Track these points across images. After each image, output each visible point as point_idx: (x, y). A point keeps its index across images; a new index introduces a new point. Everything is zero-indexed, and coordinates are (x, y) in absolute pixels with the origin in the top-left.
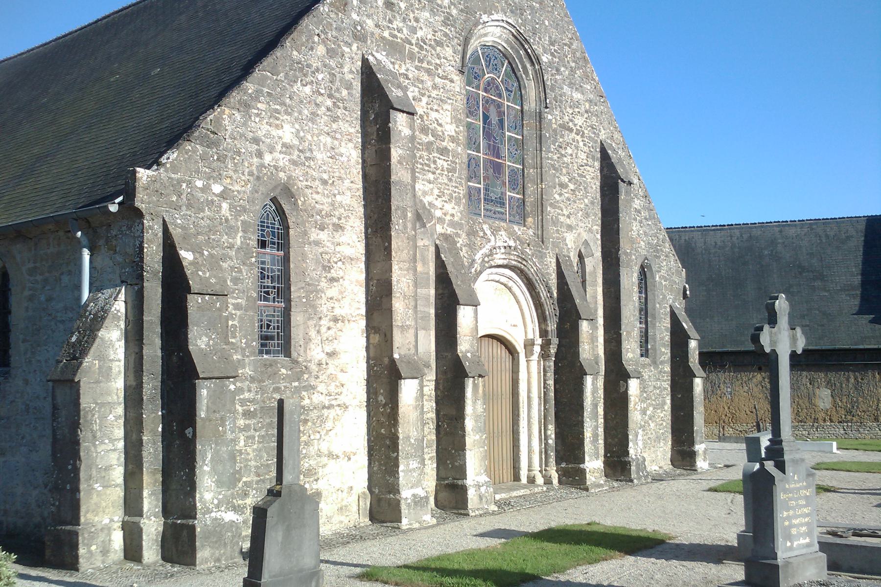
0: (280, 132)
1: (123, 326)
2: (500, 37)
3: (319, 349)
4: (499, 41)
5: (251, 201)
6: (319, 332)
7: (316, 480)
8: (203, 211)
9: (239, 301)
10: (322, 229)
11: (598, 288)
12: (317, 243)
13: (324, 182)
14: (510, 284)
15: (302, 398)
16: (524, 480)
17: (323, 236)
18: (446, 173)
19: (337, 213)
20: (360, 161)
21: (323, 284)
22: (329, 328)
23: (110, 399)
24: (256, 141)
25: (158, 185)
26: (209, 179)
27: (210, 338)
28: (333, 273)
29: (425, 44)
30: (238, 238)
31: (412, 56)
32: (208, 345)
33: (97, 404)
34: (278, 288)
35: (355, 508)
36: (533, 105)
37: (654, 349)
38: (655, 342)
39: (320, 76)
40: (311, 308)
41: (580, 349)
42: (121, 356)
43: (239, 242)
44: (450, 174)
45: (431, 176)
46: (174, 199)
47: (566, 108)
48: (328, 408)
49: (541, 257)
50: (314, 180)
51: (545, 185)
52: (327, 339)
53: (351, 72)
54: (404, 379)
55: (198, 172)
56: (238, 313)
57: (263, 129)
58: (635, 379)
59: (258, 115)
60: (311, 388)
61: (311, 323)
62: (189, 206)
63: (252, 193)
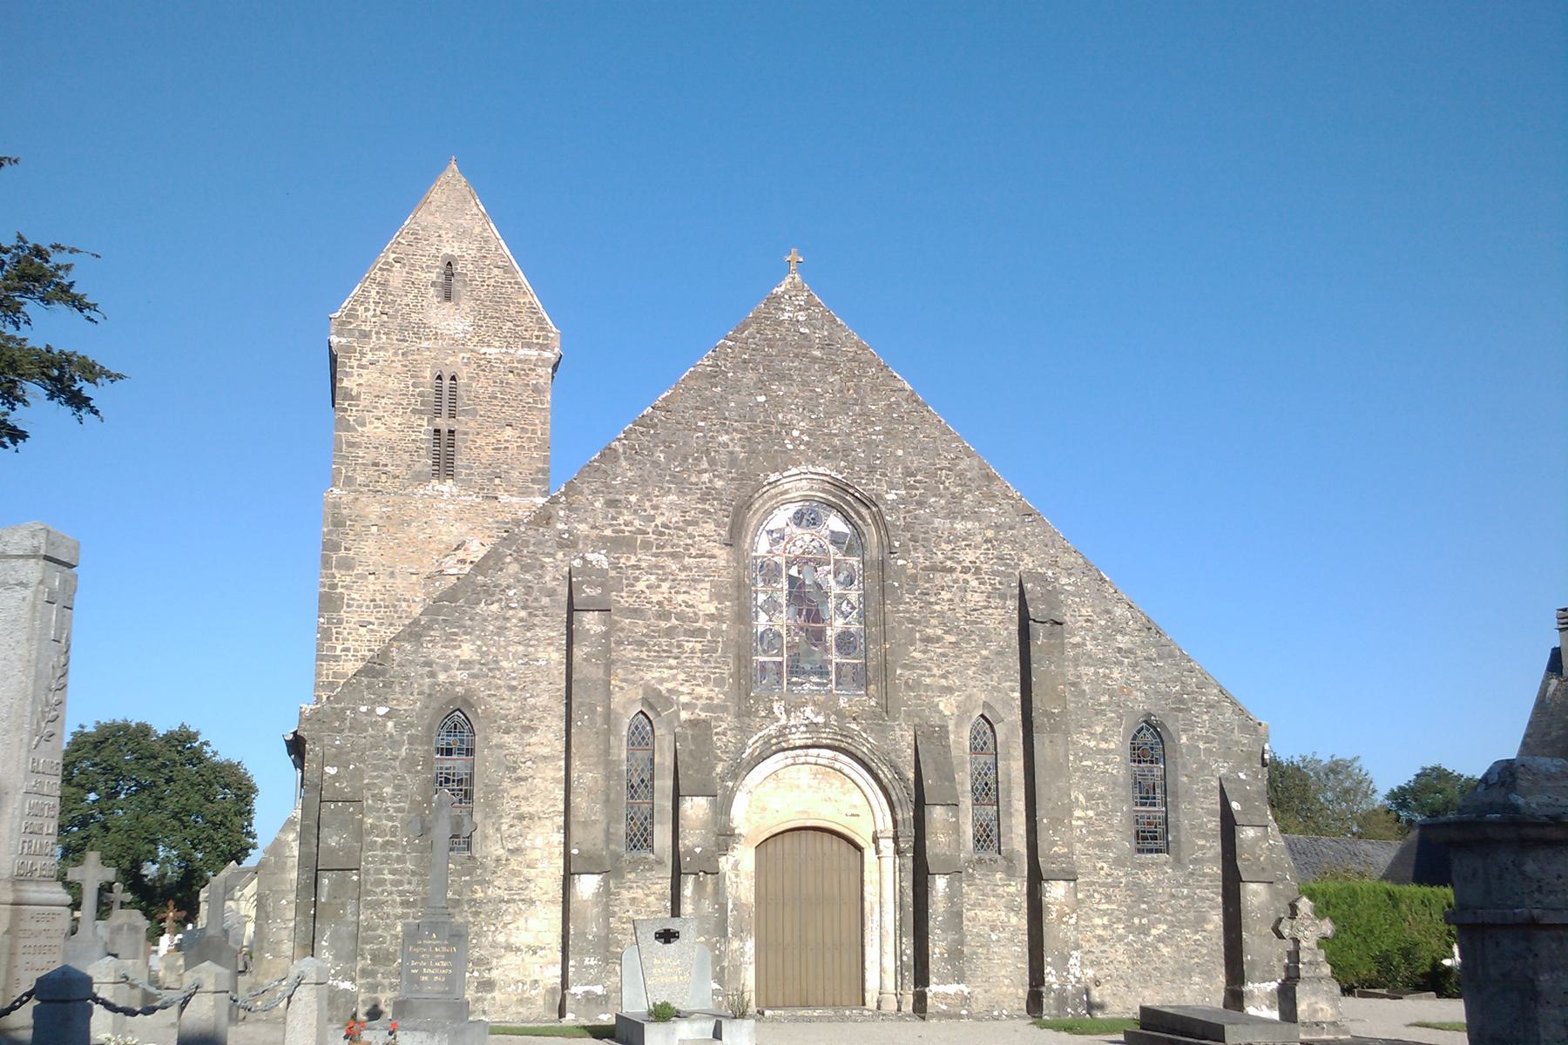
0: (458, 652)
1: (299, 830)
2: (811, 489)
3: (499, 846)
4: (813, 493)
5: (420, 716)
6: (498, 830)
7: (489, 970)
8: (366, 731)
9: (402, 804)
10: (507, 732)
11: (1012, 763)
12: (500, 746)
13: (513, 689)
14: (837, 765)
15: (475, 892)
16: (871, 1003)
17: (507, 739)
18: (699, 655)
19: (528, 716)
20: (565, 661)
21: (506, 784)
22: (511, 826)
23: (284, 888)
24: (428, 664)
25: (320, 716)
26: (374, 703)
27: (341, 837)
28: (520, 773)
29: (669, 528)
30: (403, 750)
31: (646, 545)
32: (338, 843)
33: (271, 890)
34: (466, 790)
35: (541, 1002)
36: (875, 553)
37: (1177, 841)
38: (1178, 831)
39: (511, 593)
40: (492, 808)
41: (927, 842)
42: (296, 853)
43: (404, 754)
44: (705, 655)
45: (673, 662)
46: (337, 724)
47: (938, 545)
48: (508, 902)
50: (499, 687)
51: (891, 644)
52: (509, 836)
53: (555, 579)
54: (1047, 880)
55: (362, 699)
56: (400, 815)
57: (435, 652)
58: (1062, 882)
59: (430, 641)
60: (485, 883)
61: (489, 822)
62: (351, 728)
63: (421, 709)
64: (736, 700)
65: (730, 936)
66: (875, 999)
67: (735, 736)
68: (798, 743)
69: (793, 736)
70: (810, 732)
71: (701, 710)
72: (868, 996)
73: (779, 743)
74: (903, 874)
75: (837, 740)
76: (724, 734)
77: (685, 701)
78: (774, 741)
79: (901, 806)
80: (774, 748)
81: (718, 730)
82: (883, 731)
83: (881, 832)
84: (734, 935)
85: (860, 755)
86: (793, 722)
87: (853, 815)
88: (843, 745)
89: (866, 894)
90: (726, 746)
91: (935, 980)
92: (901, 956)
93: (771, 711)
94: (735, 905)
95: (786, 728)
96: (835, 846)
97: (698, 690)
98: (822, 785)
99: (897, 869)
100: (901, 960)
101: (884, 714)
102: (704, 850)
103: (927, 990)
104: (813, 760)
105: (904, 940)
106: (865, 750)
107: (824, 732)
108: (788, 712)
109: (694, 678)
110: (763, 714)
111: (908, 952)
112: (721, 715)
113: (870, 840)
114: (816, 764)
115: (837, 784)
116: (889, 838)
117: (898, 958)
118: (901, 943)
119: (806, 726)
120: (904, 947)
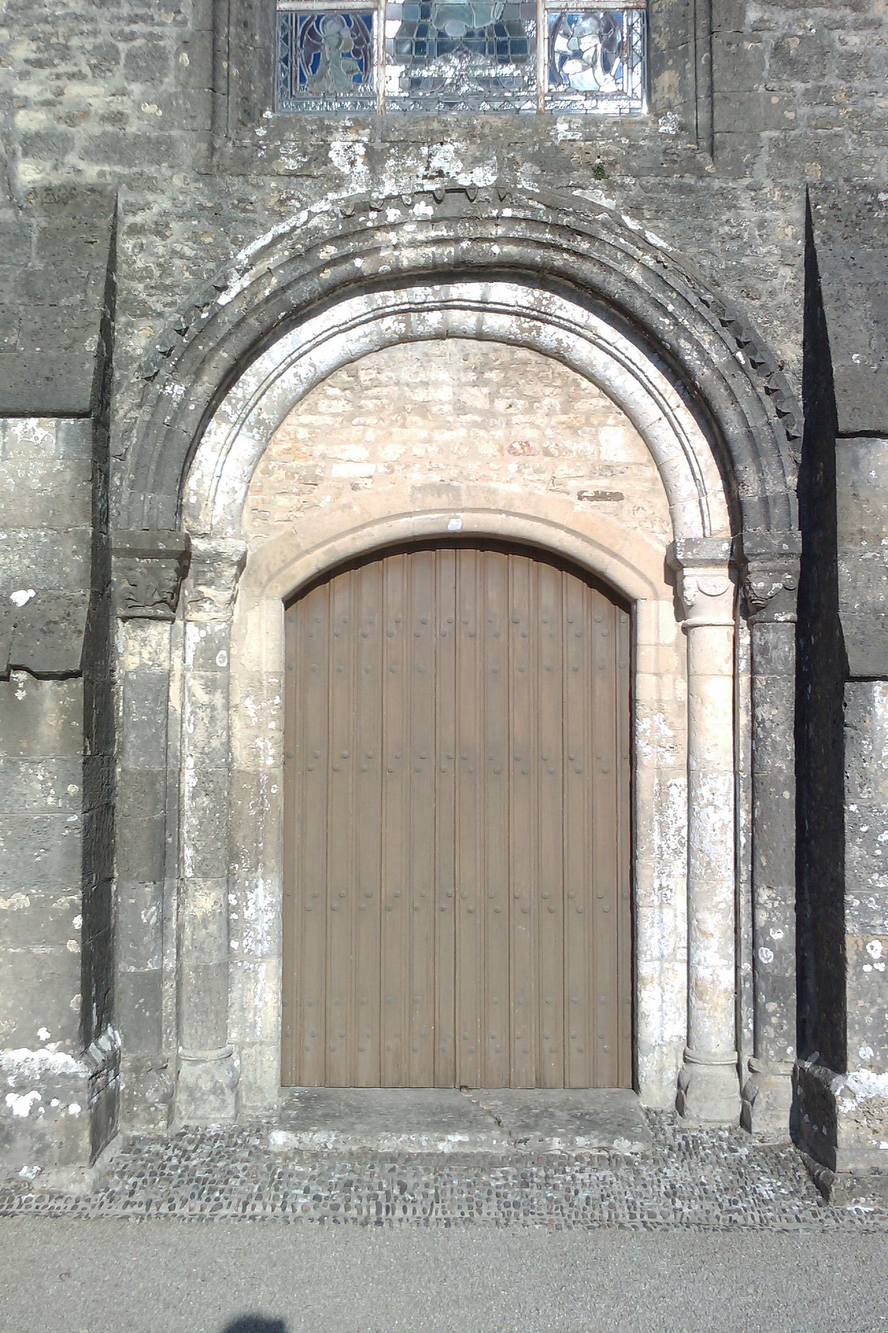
14: (549, 335)
41: (844, 569)
49: (697, 210)
64: (202, 120)
65: (189, 873)
66: (671, 1075)
67: (195, 238)
68: (408, 257)
69: (392, 237)
70: (450, 221)
71: (86, 154)
72: (647, 1065)
73: (347, 258)
74: (761, 681)
75: (540, 244)
76: (160, 230)
77: (34, 127)
78: (330, 251)
79: (757, 454)
80: (327, 274)
81: (139, 218)
82: (697, 210)
83: (690, 543)
84: (203, 871)
85: (615, 287)
86: (389, 188)
87: (600, 496)
88: (559, 260)
89: (642, 744)
90: (165, 269)
91: (866, 1052)
92: (754, 945)
93: (321, 156)
94: (204, 776)
95: (365, 206)
96: (548, 596)
97: (74, 90)
98: (500, 405)
99: (743, 665)
100: (755, 961)
101: (703, 157)
102: (45, 596)
103: (837, 1079)
104: (467, 320)
105: (764, 895)
106: (635, 273)
107: (496, 220)
108: (374, 158)
109: (65, 53)
110: (292, 165)
111: (777, 935)
112: (151, 170)
113: (658, 574)
114: (480, 337)
115: (551, 399)
116: (715, 563)
117: (745, 951)
118: (754, 903)
119: (436, 199)
120: (762, 917)
